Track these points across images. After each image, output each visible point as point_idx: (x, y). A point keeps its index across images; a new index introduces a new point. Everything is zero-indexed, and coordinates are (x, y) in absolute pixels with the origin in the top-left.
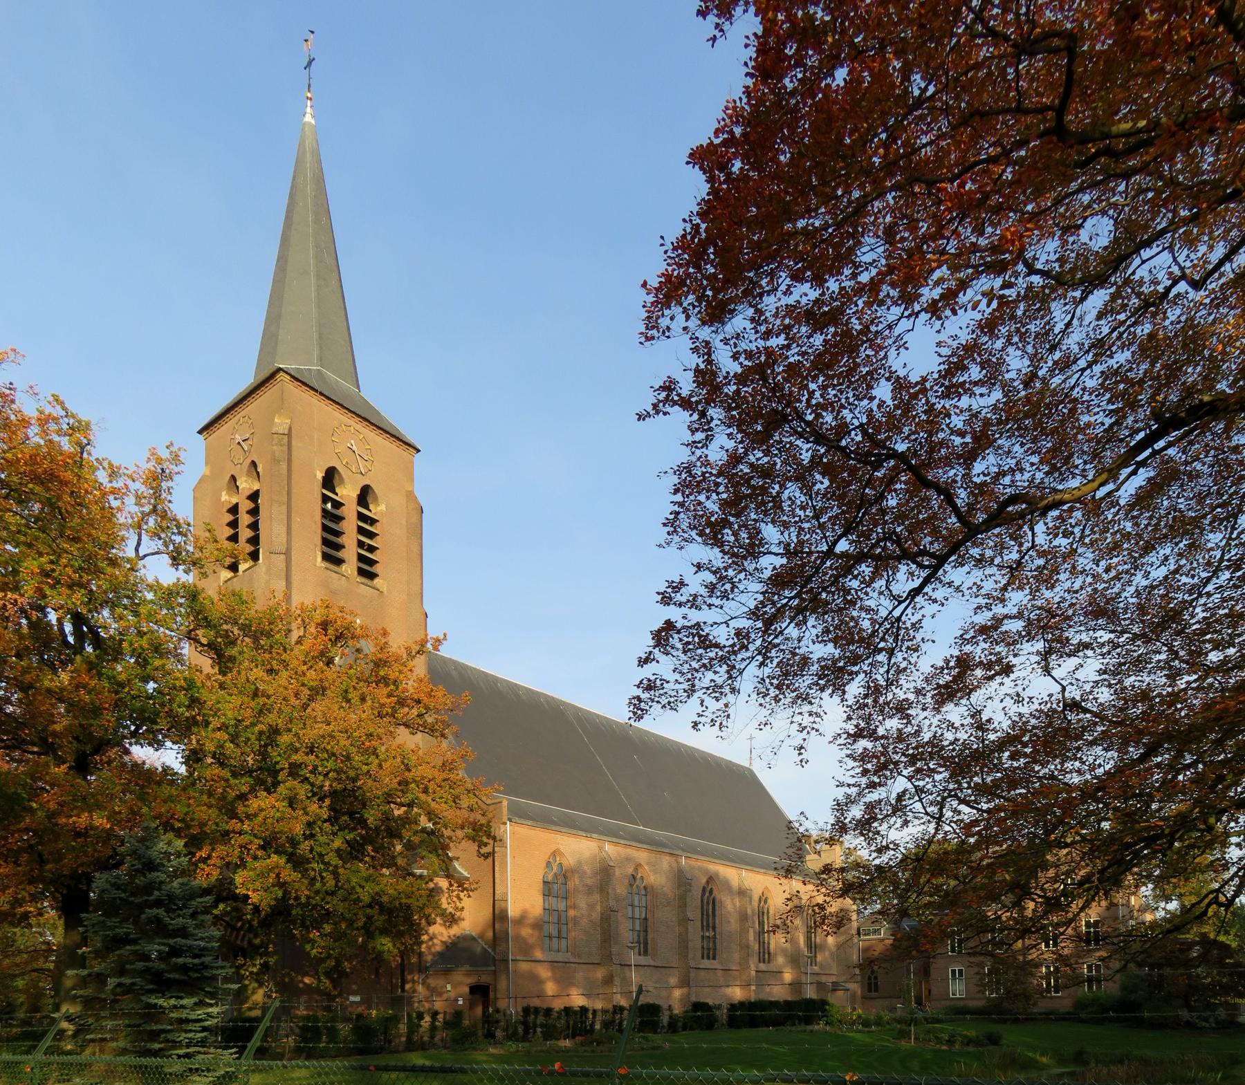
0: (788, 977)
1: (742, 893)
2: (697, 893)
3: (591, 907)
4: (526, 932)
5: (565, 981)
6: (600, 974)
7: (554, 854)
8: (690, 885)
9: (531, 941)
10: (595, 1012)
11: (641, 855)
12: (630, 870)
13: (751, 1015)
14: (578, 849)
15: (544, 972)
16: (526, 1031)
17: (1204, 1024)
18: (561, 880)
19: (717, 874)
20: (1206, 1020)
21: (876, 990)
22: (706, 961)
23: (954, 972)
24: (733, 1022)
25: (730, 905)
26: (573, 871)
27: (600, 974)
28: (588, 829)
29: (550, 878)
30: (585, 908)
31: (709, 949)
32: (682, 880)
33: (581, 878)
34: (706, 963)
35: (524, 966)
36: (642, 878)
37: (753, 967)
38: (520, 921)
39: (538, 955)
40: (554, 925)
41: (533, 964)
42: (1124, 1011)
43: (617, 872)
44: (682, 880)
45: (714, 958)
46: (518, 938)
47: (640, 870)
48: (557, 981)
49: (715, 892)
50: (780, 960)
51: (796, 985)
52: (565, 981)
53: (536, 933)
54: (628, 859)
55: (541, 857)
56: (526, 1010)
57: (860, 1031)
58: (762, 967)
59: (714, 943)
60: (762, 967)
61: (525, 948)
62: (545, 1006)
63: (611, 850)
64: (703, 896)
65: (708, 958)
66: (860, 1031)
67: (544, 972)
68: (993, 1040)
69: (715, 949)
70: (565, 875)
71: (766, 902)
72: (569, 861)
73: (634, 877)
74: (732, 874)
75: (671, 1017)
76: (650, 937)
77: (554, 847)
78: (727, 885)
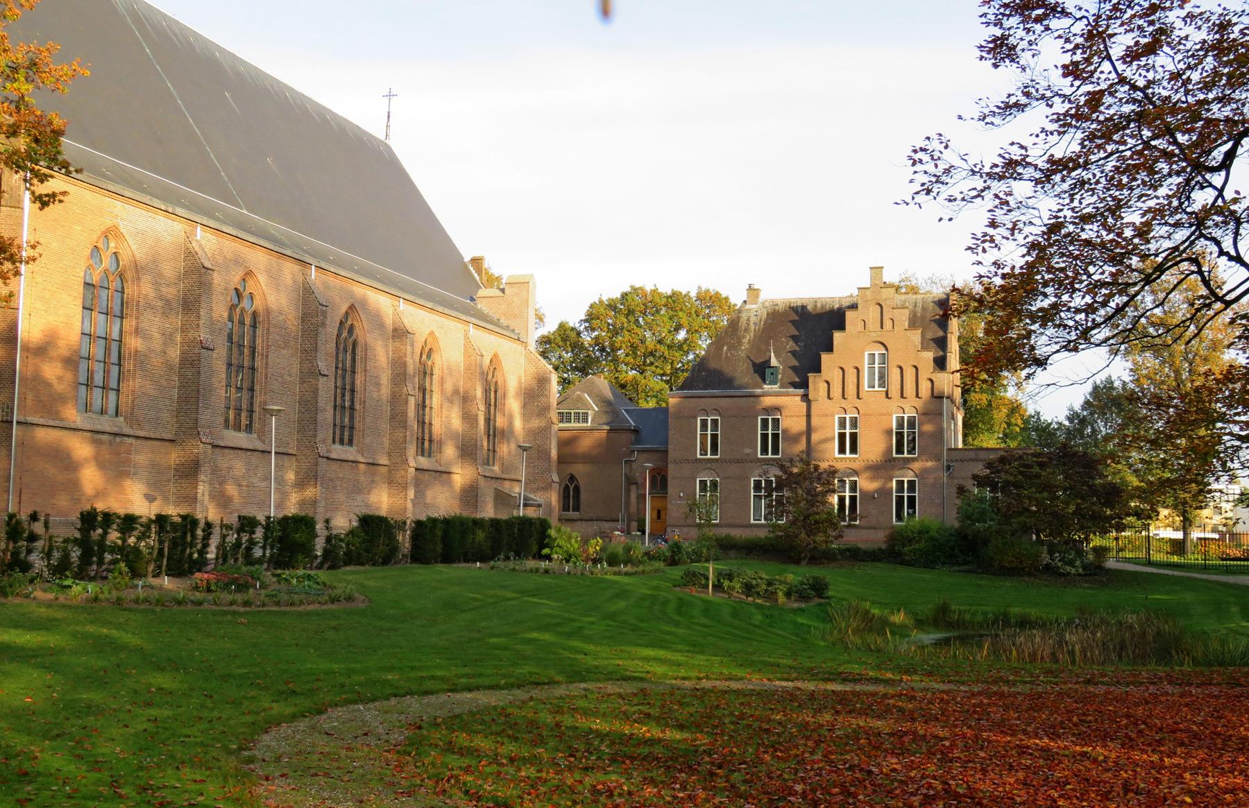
0: (461, 476)
1: (400, 333)
2: (332, 329)
3: (168, 338)
4: (51, 371)
5: (117, 469)
6: (174, 457)
7: (106, 235)
8: (324, 314)
9: (60, 388)
10: (209, 525)
11: (258, 259)
12: (236, 280)
13: (443, 541)
14: (150, 230)
15: (81, 448)
16: (85, 559)
17: (1068, 568)
18: (116, 284)
19: (364, 302)
20: (1071, 563)
21: (577, 509)
22: (337, 446)
23: (703, 483)
24: (419, 555)
25: (380, 354)
26: (138, 268)
27: (174, 457)
28: (169, 201)
29: (95, 279)
30: (154, 337)
31: (343, 427)
32: (311, 307)
33: (156, 284)
34: (338, 451)
35: (43, 435)
36: (251, 296)
37: (412, 463)
38: (41, 351)
39: (72, 414)
40: (102, 366)
41: (66, 433)
42: (962, 549)
43: (217, 278)
44: (311, 307)
45: (350, 443)
46: (37, 381)
47: (250, 283)
48: (101, 465)
49: (358, 331)
50: (450, 451)
51: (470, 494)
52: (117, 469)
53: (69, 376)
54: (237, 261)
55: (83, 237)
56: (89, 519)
57: (626, 574)
58: (424, 462)
59: (352, 418)
60: (424, 462)
61: (49, 404)
62: (122, 512)
63: (205, 241)
64: (338, 336)
65: (342, 442)
66: (626, 574)
67: (81, 448)
68: (819, 588)
69: (352, 428)
70: (122, 274)
71: (429, 356)
72: (133, 249)
73: (239, 294)
74: (383, 303)
75: (328, 539)
76: (258, 399)
77: (108, 223)
78: (377, 320)
